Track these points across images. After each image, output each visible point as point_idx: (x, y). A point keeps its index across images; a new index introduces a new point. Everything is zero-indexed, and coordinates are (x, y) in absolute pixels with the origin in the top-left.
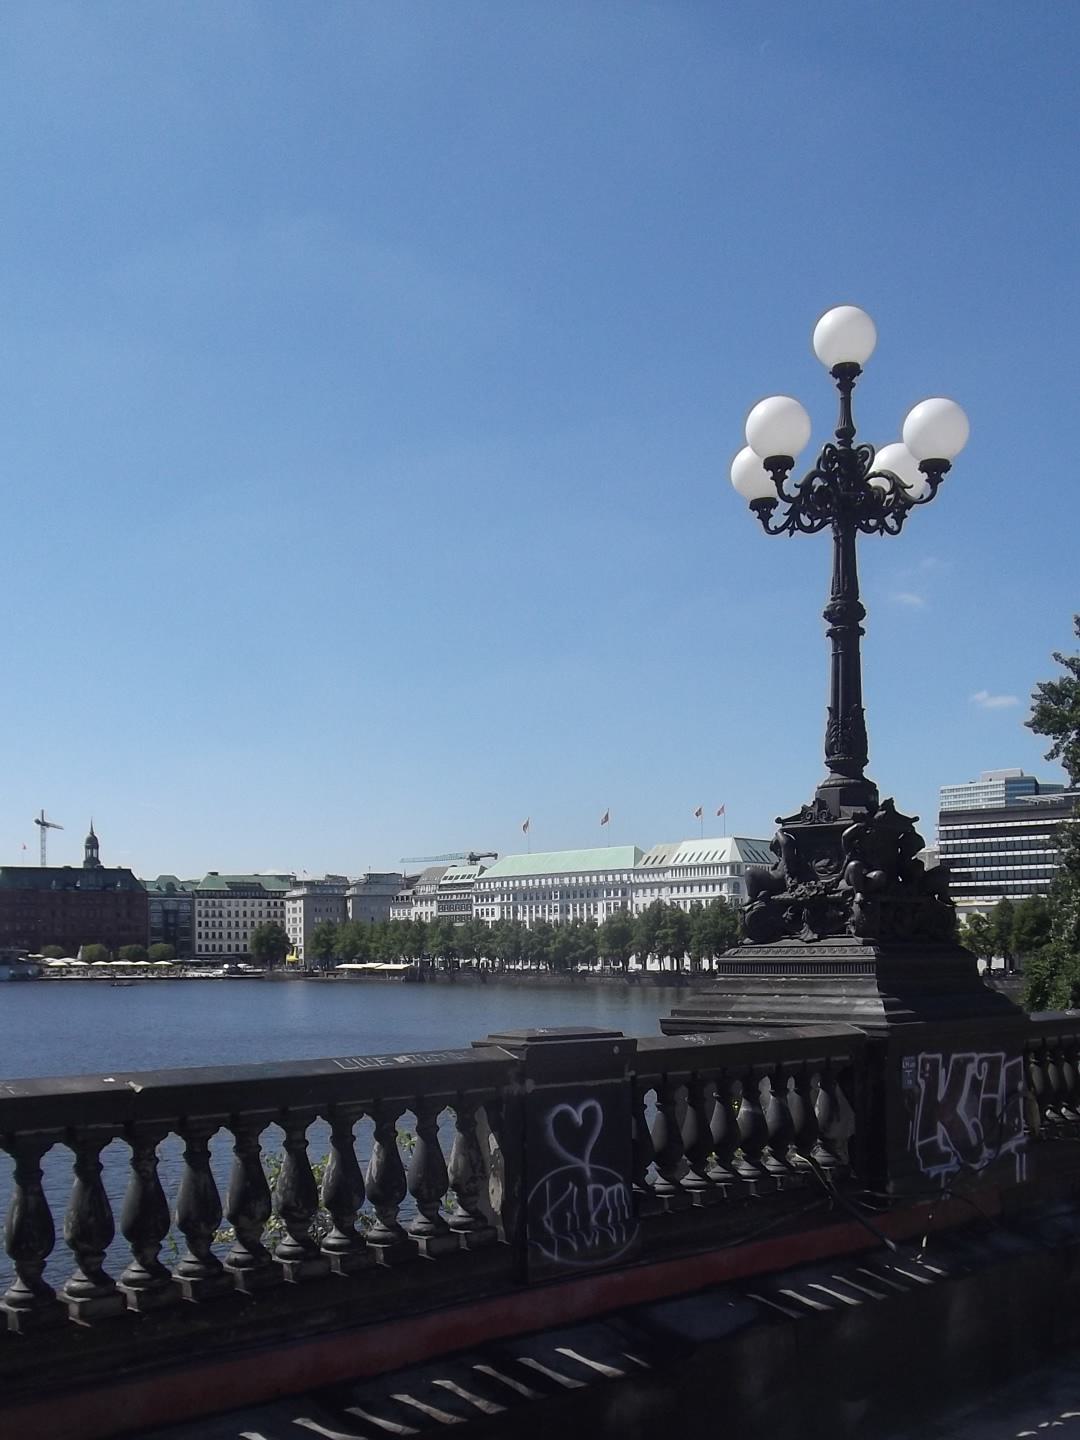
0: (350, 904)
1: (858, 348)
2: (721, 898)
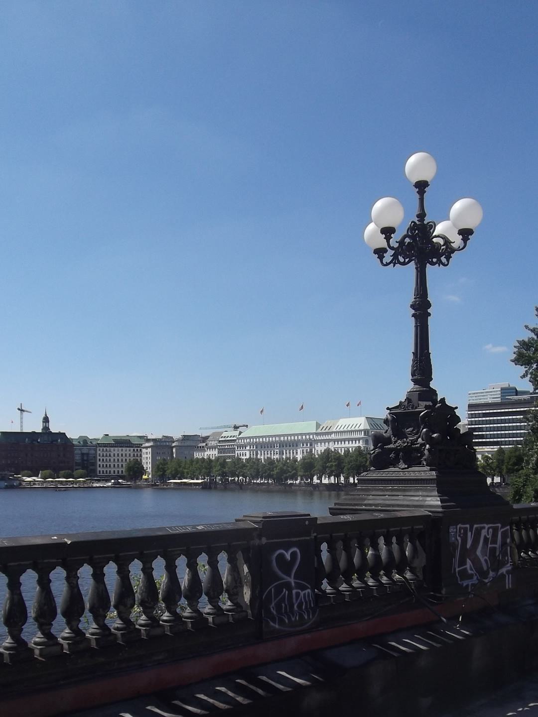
0: (174, 450)
1: (428, 173)
2: (359, 447)
